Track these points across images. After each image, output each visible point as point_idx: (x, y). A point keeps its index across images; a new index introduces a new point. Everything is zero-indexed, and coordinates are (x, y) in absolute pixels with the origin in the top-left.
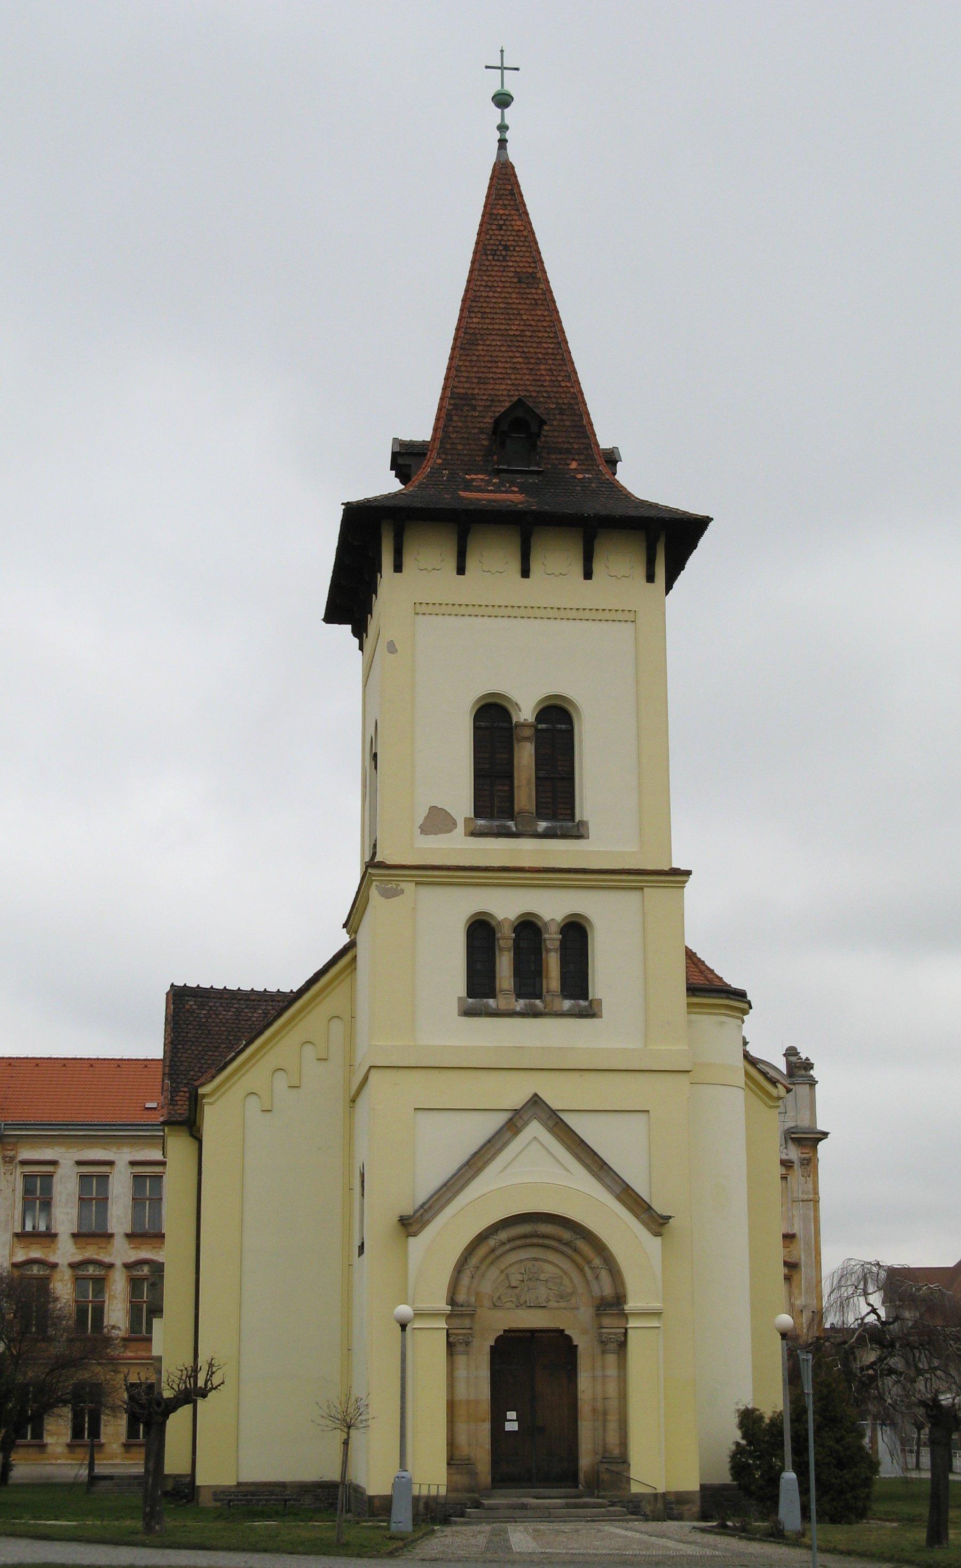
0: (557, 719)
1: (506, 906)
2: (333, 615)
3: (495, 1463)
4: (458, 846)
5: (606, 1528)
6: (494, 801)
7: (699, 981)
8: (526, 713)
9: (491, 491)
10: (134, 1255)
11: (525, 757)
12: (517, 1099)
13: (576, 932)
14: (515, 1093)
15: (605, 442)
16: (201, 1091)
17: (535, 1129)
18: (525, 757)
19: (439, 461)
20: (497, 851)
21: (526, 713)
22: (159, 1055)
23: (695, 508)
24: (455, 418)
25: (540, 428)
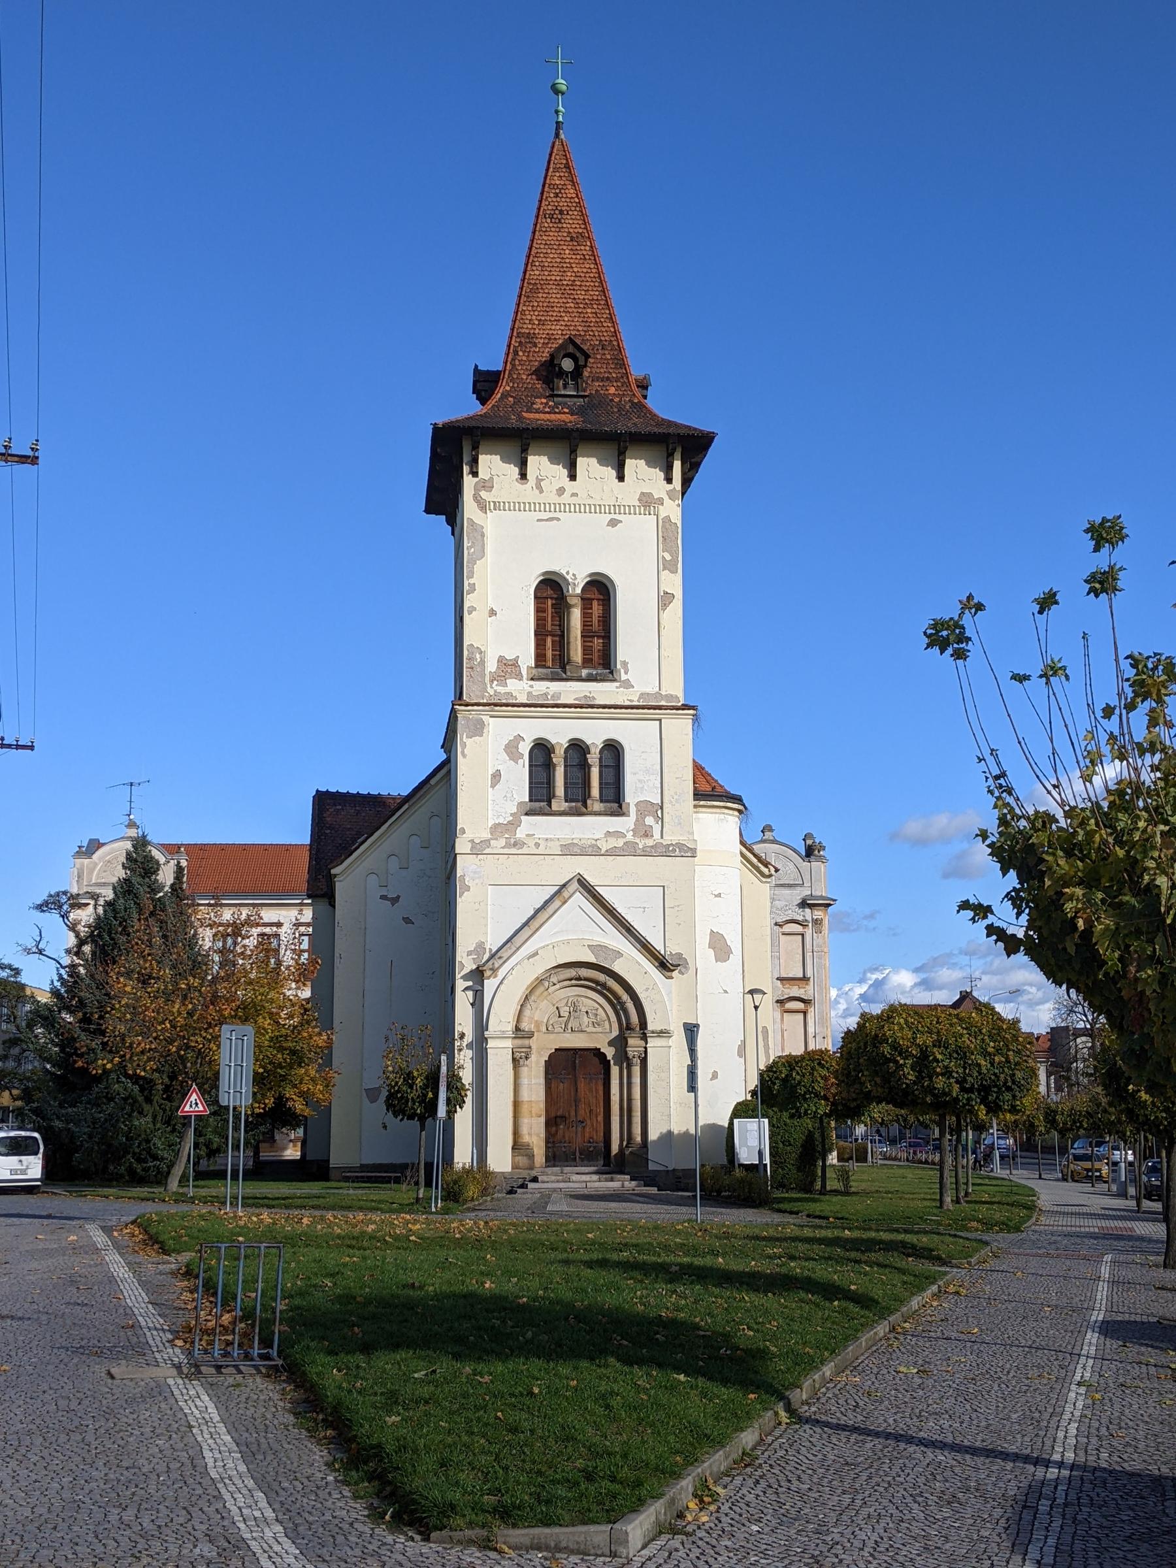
0: (600, 590)
1: (560, 732)
2: (432, 507)
3: (552, 1122)
4: (519, 689)
6: (553, 657)
7: (705, 787)
13: (613, 750)
15: (636, 371)
16: (333, 871)
17: (579, 899)
22: (308, 841)
23: (706, 427)
24: (521, 353)
25: (586, 361)
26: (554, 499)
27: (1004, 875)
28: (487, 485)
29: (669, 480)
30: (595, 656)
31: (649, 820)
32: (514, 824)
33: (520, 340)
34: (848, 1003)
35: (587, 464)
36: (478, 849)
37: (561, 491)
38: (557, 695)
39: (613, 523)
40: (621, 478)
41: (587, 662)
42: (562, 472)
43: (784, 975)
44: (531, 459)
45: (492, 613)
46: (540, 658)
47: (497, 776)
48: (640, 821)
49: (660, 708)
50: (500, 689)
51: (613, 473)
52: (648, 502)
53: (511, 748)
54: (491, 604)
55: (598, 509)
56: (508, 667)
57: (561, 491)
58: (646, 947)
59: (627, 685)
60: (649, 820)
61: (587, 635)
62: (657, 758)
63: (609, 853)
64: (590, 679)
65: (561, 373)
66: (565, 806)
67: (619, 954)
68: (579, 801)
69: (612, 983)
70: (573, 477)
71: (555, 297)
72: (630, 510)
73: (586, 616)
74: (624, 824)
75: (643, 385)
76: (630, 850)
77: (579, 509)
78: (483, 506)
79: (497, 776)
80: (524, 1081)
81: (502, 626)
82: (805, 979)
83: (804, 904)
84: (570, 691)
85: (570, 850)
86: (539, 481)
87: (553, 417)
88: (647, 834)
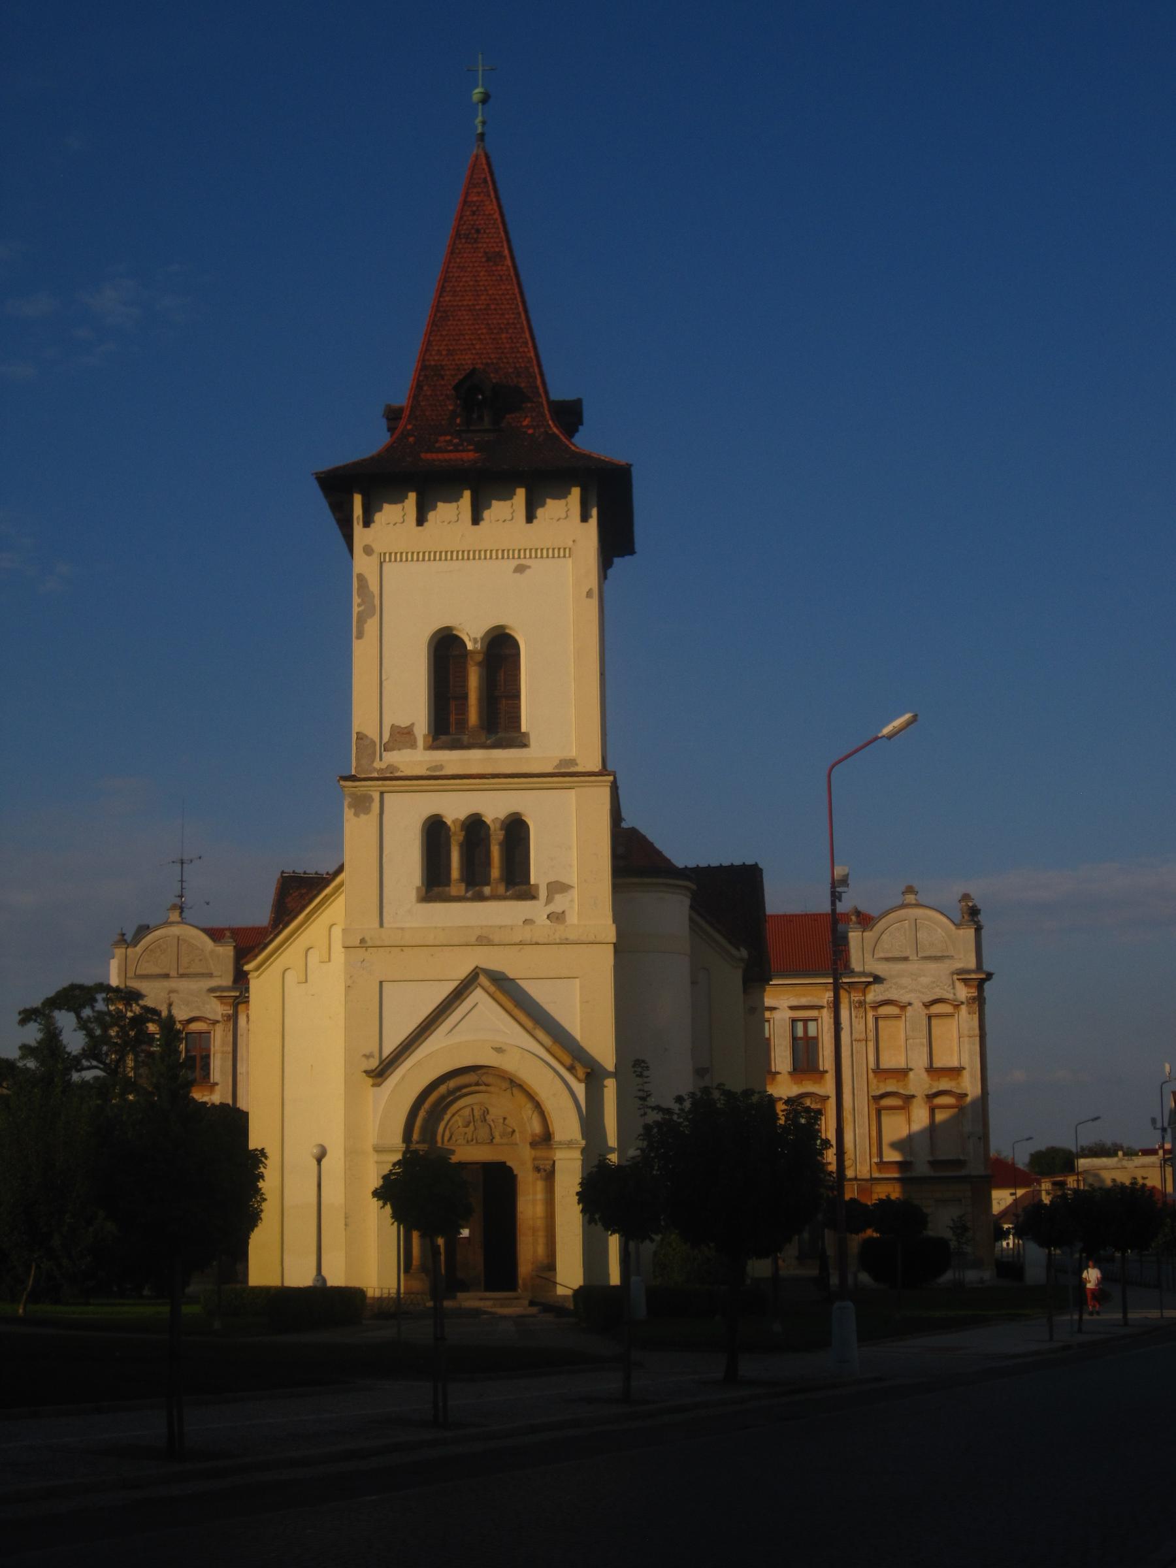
0: (501, 649)
1: (455, 807)
5: (472, 456)
6: (446, 726)
9: (450, 451)
12: (463, 972)
13: (516, 828)
19: (409, 427)
20: (453, 760)
24: (425, 388)
27: (413, 724)
33: (427, 373)
34: (585, 1066)
39: (520, 569)
56: (402, 737)
68: (475, 883)
74: (536, 910)
80: (540, 1210)
81: (391, 687)
84: (475, 759)
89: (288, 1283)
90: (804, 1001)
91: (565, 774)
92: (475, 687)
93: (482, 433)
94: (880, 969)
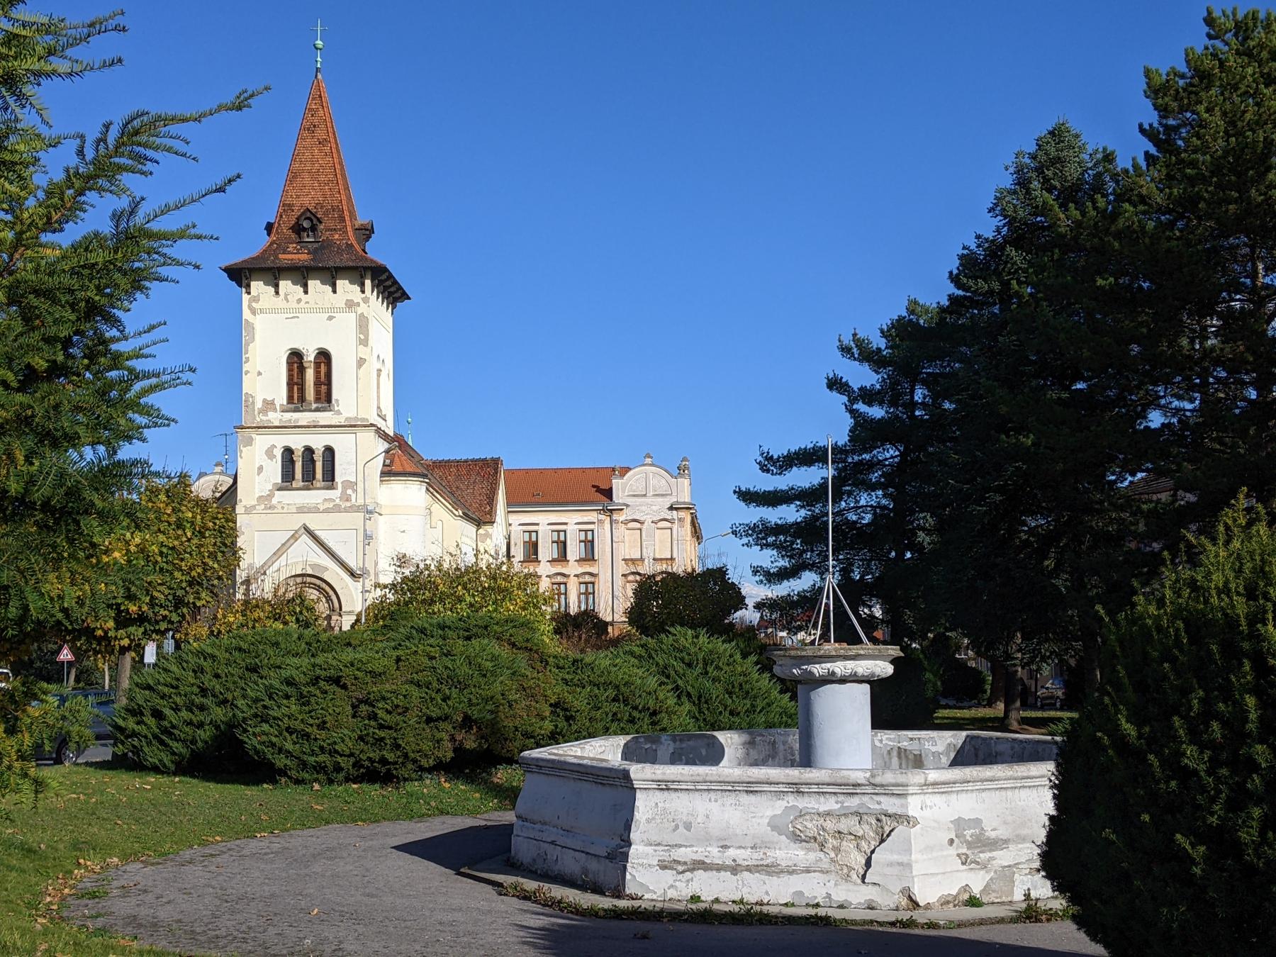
0: (324, 357)
1: (298, 442)
4: (275, 417)
5: (304, 257)
6: (296, 396)
8: (310, 357)
10: (580, 570)
11: (310, 375)
13: (329, 452)
14: (297, 522)
17: (305, 538)
18: (310, 375)
21: (310, 357)
26: (295, 305)
28: (256, 299)
29: (363, 292)
30: (323, 395)
31: (349, 492)
32: (271, 496)
33: (287, 207)
35: (314, 284)
36: (249, 510)
37: (299, 301)
38: (297, 420)
39: (330, 318)
40: (335, 292)
41: (317, 400)
42: (300, 289)
43: (658, 556)
44: (281, 283)
45: (259, 374)
46: (290, 398)
47: (260, 469)
48: (344, 492)
49: (354, 426)
50: (264, 418)
51: (330, 289)
52: (350, 305)
53: (269, 453)
54: (259, 368)
55: (322, 310)
56: (269, 405)
57: (299, 301)
58: (343, 565)
59: (339, 413)
60: (349, 492)
61: (318, 383)
62: (359, 456)
63: (326, 511)
64: (317, 410)
65: (305, 229)
66: (302, 484)
67: (326, 569)
69: (324, 585)
70: (306, 292)
71: (307, 181)
72: (341, 310)
73: (317, 372)
74: (334, 494)
75: (366, 232)
76: (337, 509)
77: (311, 311)
78: (253, 312)
79: (260, 469)
81: (264, 379)
82: (672, 559)
83: (671, 508)
84: (304, 418)
85: (301, 510)
86: (286, 295)
87: (297, 256)
88: (348, 499)
89: (639, 795)
90: (585, 519)
91: (351, 426)
92: (310, 379)
93: (314, 247)
94: (629, 501)
